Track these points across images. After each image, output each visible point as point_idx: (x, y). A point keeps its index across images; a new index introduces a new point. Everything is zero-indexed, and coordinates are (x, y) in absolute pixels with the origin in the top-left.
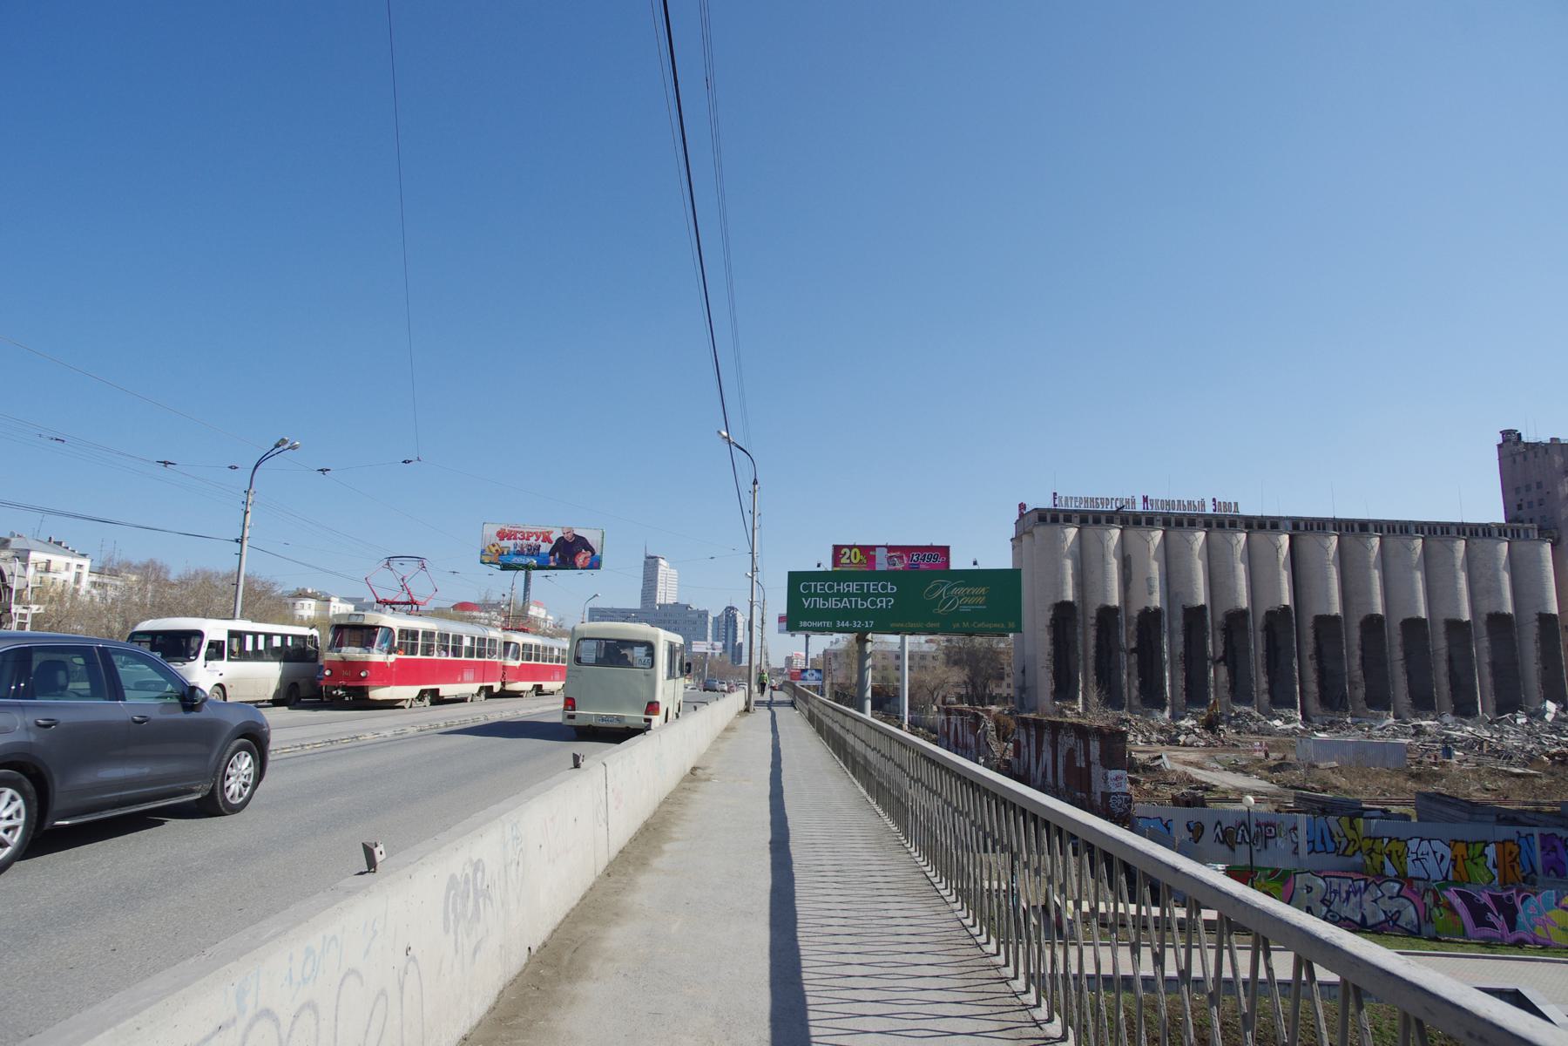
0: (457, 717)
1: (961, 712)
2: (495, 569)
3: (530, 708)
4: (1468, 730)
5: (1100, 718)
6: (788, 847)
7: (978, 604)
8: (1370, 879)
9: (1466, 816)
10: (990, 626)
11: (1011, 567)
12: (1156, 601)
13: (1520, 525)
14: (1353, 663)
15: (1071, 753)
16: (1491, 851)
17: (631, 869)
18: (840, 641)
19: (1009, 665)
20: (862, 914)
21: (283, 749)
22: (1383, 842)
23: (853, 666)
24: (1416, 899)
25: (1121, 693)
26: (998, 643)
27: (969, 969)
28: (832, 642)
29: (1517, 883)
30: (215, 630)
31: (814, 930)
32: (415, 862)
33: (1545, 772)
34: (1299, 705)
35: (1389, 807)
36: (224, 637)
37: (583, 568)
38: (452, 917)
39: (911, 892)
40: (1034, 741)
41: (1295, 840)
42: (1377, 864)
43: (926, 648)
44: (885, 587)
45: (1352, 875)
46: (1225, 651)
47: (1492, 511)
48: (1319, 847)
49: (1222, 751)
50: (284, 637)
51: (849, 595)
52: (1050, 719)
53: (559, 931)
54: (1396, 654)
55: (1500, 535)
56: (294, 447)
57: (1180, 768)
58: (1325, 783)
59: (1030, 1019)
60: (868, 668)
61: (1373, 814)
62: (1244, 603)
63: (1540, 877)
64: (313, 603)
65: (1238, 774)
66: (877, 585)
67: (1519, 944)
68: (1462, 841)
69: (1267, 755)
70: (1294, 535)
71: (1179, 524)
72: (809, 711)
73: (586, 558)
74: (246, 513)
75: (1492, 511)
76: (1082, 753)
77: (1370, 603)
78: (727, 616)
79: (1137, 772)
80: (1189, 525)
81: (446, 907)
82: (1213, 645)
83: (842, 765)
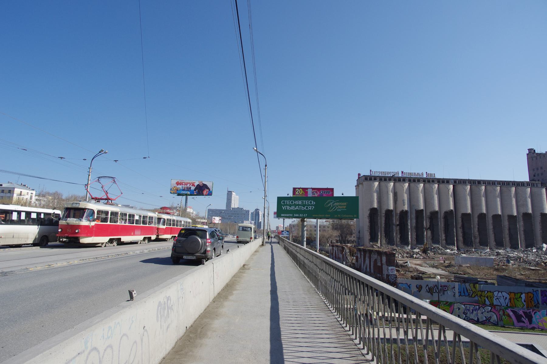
1: (337, 246)
2: (175, 195)
5: (386, 248)
9: (515, 284)
10: (348, 216)
11: (355, 196)
12: (406, 208)
13: (534, 182)
14: (475, 231)
15: (376, 260)
16: (523, 296)
17: (222, 300)
18: (295, 221)
19: (354, 230)
20: (302, 316)
22: (485, 293)
24: (497, 313)
25: (394, 238)
27: (339, 336)
31: (285, 321)
33: (543, 268)
34: (456, 244)
35: (487, 280)
37: (206, 195)
38: (159, 316)
43: (325, 224)
44: (311, 202)
46: (430, 226)
47: (525, 177)
49: (429, 260)
51: (298, 205)
52: (368, 249)
54: (490, 227)
55: (527, 185)
56: (106, 153)
57: (414, 266)
59: (361, 353)
60: (305, 231)
61: (481, 283)
62: (437, 208)
63: (541, 305)
67: (533, 329)
68: (513, 293)
69: (444, 262)
71: (414, 181)
72: (284, 245)
73: (207, 192)
74: (89, 175)
75: (525, 177)
76: (380, 261)
77: (481, 209)
78: (256, 212)
79: (399, 267)
82: (426, 223)
83: (296, 264)
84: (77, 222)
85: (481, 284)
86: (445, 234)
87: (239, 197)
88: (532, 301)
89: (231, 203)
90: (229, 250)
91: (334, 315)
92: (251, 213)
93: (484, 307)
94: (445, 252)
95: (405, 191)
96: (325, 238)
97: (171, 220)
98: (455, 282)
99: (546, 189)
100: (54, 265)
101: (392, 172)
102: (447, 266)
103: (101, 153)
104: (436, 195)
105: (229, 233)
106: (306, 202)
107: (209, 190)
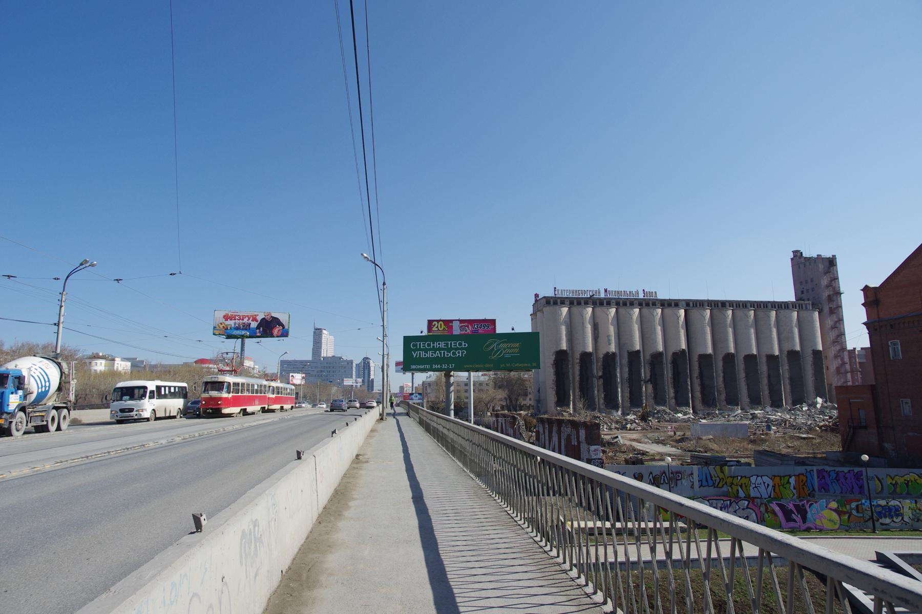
0: (206, 430)
1: (504, 416)
2: (223, 338)
3: (250, 423)
4: (778, 415)
5: (584, 416)
6: (423, 500)
7: (515, 353)
8: (733, 500)
9: (780, 462)
10: (521, 365)
11: (531, 331)
12: (613, 348)
13: (803, 302)
14: (719, 381)
15: (569, 437)
16: (792, 480)
17: (332, 519)
18: (431, 376)
19: (530, 387)
20: (475, 538)
21: (96, 455)
22: (738, 479)
23: (440, 391)
24: (756, 509)
25: (594, 399)
26: (524, 375)
27: (543, 567)
28: (427, 377)
29: (806, 497)
30: (151, 385)
31: (449, 549)
32: (224, 524)
33: (817, 435)
34: (691, 404)
35: (740, 459)
36: (154, 389)
37: (278, 337)
38: (244, 556)
39: (500, 523)
40: (547, 431)
41: (692, 480)
42: (735, 490)
43: (482, 379)
44: (460, 344)
45: (722, 498)
46: (651, 376)
47: (788, 294)
48: (705, 483)
49: (651, 432)
50: (175, 387)
51: (439, 349)
52: (556, 418)
53: (297, 559)
54: (742, 375)
55: (793, 308)
56: (92, 265)
57: (628, 443)
58: (707, 448)
59: (583, 593)
60: (452, 392)
61: (732, 463)
62: (661, 348)
63: (817, 493)
64: (103, 362)
65: (660, 445)
66: (456, 343)
67: (808, 530)
68: (778, 476)
69: (675, 434)
70: (687, 310)
71: (625, 304)
72: (420, 418)
73: (279, 330)
74: (61, 306)
75: (788, 294)
76: (575, 437)
77: (727, 347)
78: (364, 363)
79: (605, 446)
80: (585, 304)
81: (241, 549)
82: (645, 373)
83: (445, 450)
84: (219, 395)
85: (732, 466)
86: (674, 388)
87: (334, 337)
88: (805, 487)
89: (321, 348)
90: (335, 430)
91: (527, 533)
92: (356, 364)
93: (738, 502)
94: (675, 417)
95: (610, 321)
96: (483, 403)
97: (239, 383)
98: (692, 464)
99: (819, 313)
100: (4, 476)
101: (590, 291)
102: (679, 439)
103: (84, 266)
104: (660, 325)
105: (320, 401)
106: (453, 345)
107: (284, 327)
